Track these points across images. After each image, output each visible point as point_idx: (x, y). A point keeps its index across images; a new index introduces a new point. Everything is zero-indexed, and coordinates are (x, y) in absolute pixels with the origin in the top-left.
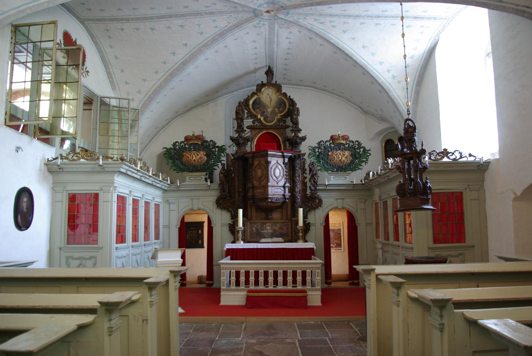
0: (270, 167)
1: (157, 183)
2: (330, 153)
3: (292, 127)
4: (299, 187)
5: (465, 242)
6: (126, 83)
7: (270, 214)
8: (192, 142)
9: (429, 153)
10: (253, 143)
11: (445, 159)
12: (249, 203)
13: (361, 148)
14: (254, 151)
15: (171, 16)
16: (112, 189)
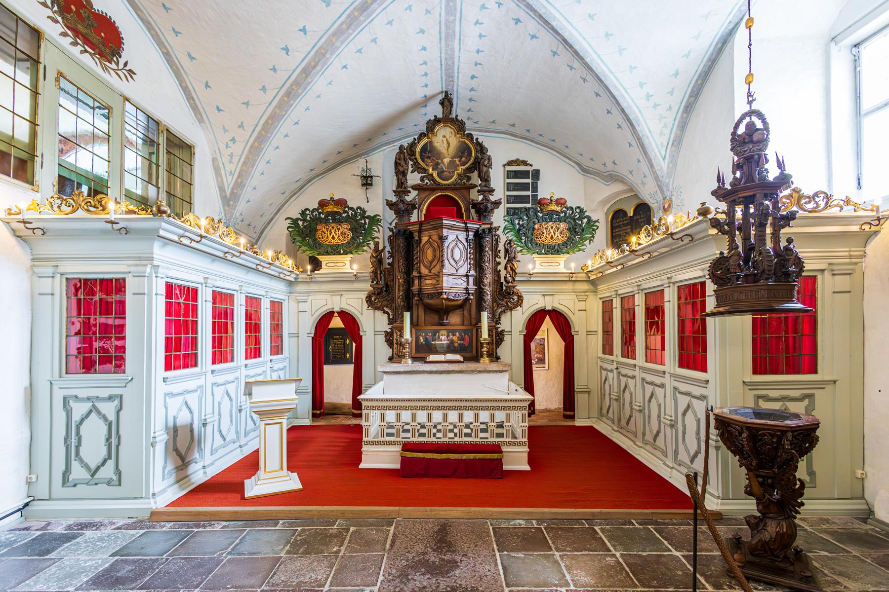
0: (446, 245)
1: (263, 267)
2: (536, 227)
4: (488, 279)
5: (814, 371)
7: (445, 318)
8: (329, 210)
10: (422, 211)
12: (414, 301)
13: (584, 218)
14: (423, 219)
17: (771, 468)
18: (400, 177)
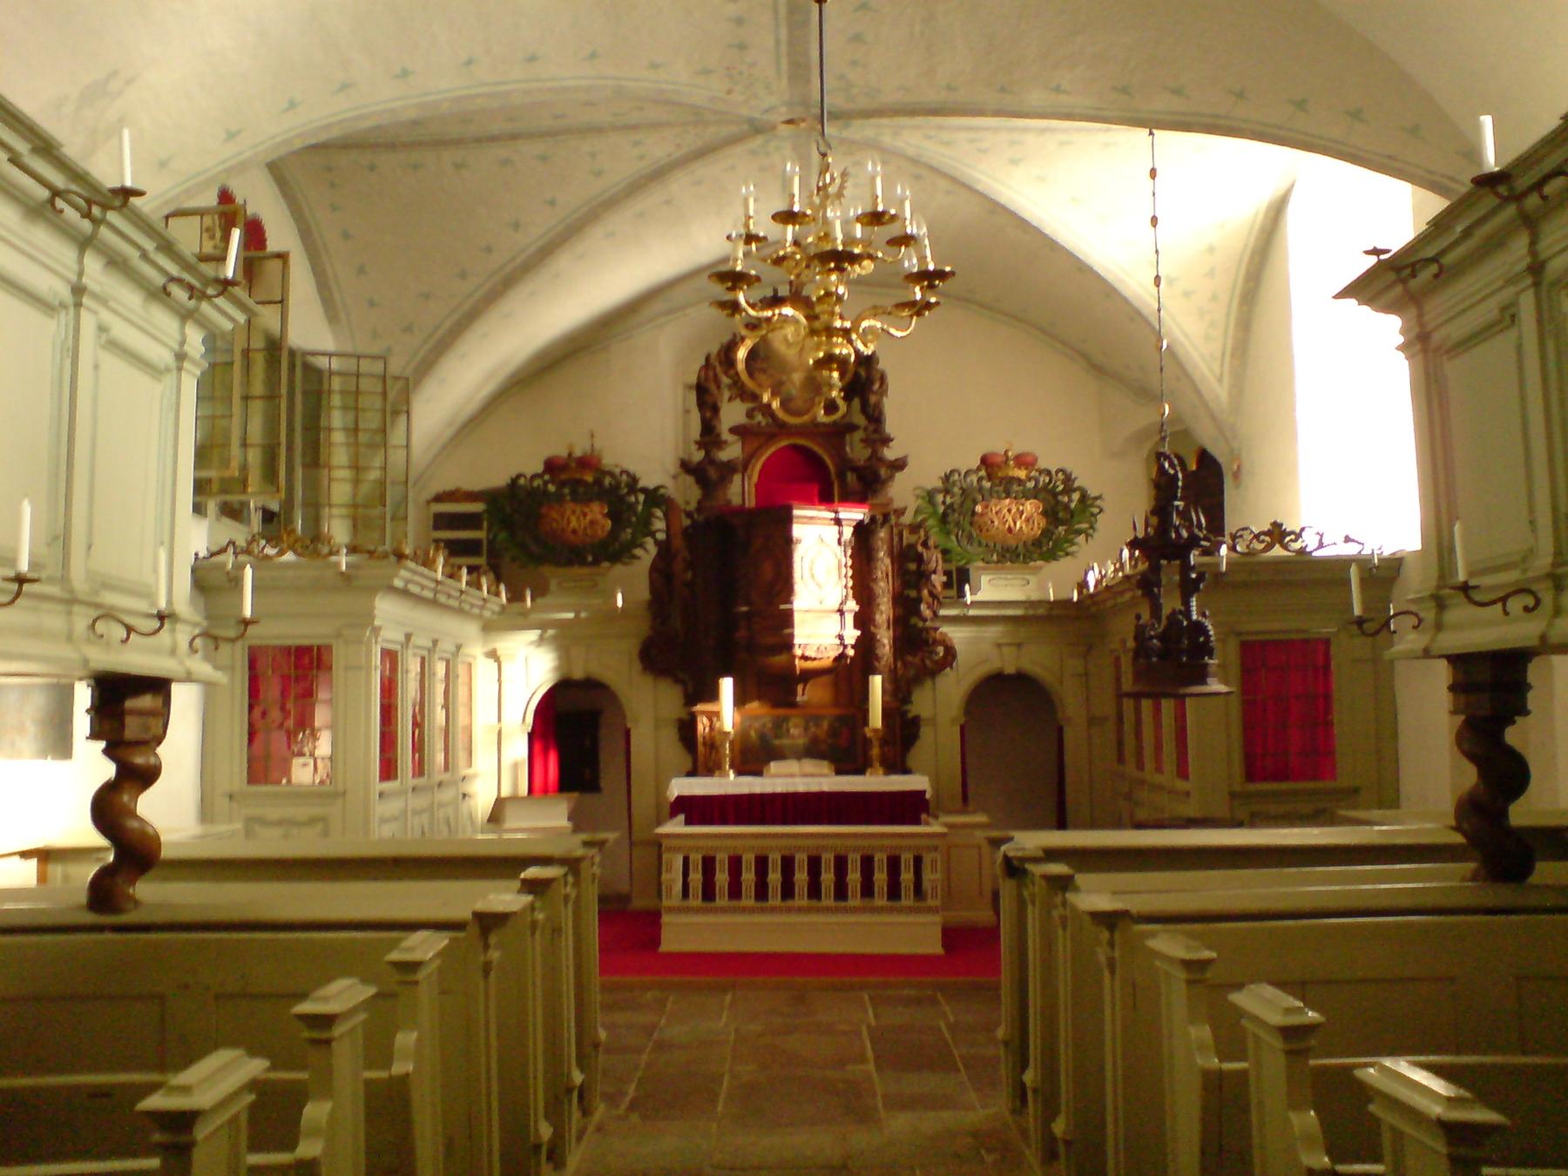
2: (979, 509)
3: (866, 429)
5: (1333, 776)
6: (371, 304)
9: (1231, 534)
11: (1277, 551)
13: (1075, 490)
15: (514, 137)
16: (368, 634)
17: (353, 549)
18: (708, 415)
